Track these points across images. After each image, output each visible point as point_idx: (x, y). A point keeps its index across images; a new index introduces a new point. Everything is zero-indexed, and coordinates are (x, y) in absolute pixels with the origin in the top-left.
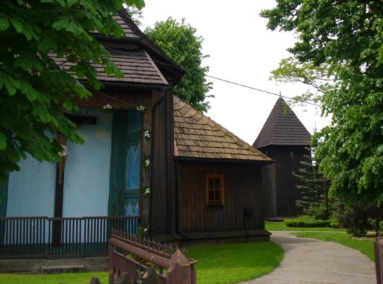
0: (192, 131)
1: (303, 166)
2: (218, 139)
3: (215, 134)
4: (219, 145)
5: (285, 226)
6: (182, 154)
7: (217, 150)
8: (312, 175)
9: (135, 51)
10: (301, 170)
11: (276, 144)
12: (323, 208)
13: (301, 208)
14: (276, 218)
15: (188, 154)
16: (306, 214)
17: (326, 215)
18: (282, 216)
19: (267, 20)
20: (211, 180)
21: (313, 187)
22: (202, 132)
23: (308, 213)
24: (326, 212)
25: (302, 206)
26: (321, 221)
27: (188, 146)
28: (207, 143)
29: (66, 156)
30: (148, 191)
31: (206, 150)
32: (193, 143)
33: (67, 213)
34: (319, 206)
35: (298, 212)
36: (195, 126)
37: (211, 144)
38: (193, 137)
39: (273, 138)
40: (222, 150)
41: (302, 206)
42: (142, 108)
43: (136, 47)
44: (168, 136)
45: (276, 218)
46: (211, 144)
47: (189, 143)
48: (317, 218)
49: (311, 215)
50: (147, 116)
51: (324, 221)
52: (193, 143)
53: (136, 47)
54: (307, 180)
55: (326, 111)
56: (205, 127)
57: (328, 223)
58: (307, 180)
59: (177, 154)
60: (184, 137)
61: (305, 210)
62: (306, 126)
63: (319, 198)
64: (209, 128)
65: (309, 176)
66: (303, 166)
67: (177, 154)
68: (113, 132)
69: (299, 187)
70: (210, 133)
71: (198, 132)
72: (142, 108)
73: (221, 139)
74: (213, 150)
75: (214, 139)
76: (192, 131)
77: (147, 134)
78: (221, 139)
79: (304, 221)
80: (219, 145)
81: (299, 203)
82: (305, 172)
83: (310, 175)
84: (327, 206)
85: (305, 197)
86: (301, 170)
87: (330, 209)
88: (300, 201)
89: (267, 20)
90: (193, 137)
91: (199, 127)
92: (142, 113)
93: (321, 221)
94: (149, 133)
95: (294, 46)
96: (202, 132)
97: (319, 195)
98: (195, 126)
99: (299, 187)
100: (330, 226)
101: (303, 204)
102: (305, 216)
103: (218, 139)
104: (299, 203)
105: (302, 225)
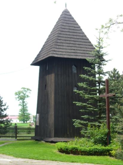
1: (83, 80)
5: (56, 151)
8: (95, 90)
10: (81, 84)
11: (56, 56)
12: (104, 129)
13: (79, 129)
14: (53, 139)
16: (84, 136)
17: (106, 140)
18: (59, 137)
19: (116, 69)
21: (94, 104)
23: (86, 135)
24: (108, 134)
25: (80, 126)
26: (100, 147)
34: (99, 126)
35: (76, 133)
39: (53, 49)
41: (80, 126)
45: (53, 139)
48: (96, 142)
49: (89, 137)
51: (103, 147)
54: (87, 96)
57: (108, 151)
58: (87, 96)
61: (82, 132)
62: (88, 36)
63: (100, 118)
65: (90, 92)
66: (83, 80)
69: (78, 104)
79: (78, 146)
81: (77, 123)
82: (85, 86)
83: (91, 91)
84: (109, 128)
85: (86, 117)
86: (81, 84)
87: (113, 132)
88: (79, 121)
89: (116, 69)
93: (100, 147)
97: (100, 114)
99: (78, 104)
100: (110, 155)
101: (80, 123)
102: (83, 139)
104: (77, 123)
105: (75, 152)
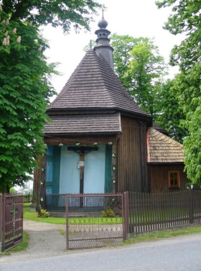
0: (161, 148)
2: (176, 151)
3: (175, 148)
4: (177, 154)
6: (152, 161)
7: (174, 158)
9: (114, 113)
15: (156, 161)
20: (171, 174)
22: (167, 148)
27: (157, 156)
28: (169, 154)
29: (84, 166)
30: (114, 182)
31: (167, 158)
32: (160, 155)
33: (86, 191)
36: (163, 145)
37: (172, 154)
38: (161, 151)
40: (178, 158)
42: (111, 143)
43: (114, 112)
44: (142, 152)
46: (172, 154)
47: (157, 155)
50: (114, 147)
52: (160, 155)
53: (114, 112)
55: (142, 133)
56: (169, 145)
59: (149, 161)
60: (155, 151)
64: (172, 145)
67: (149, 161)
68: (106, 156)
70: (172, 148)
71: (164, 148)
72: (111, 143)
73: (179, 151)
74: (172, 158)
75: (174, 151)
76: (161, 148)
77: (113, 155)
78: (179, 151)
80: (177, 154)
90: (161, 151)
91: (165, 145)
92: (111, 146)
94: (115, 154)
95: (48, 62)
96: (167, 148)
98: (163, 145)
103: (176, 151)
